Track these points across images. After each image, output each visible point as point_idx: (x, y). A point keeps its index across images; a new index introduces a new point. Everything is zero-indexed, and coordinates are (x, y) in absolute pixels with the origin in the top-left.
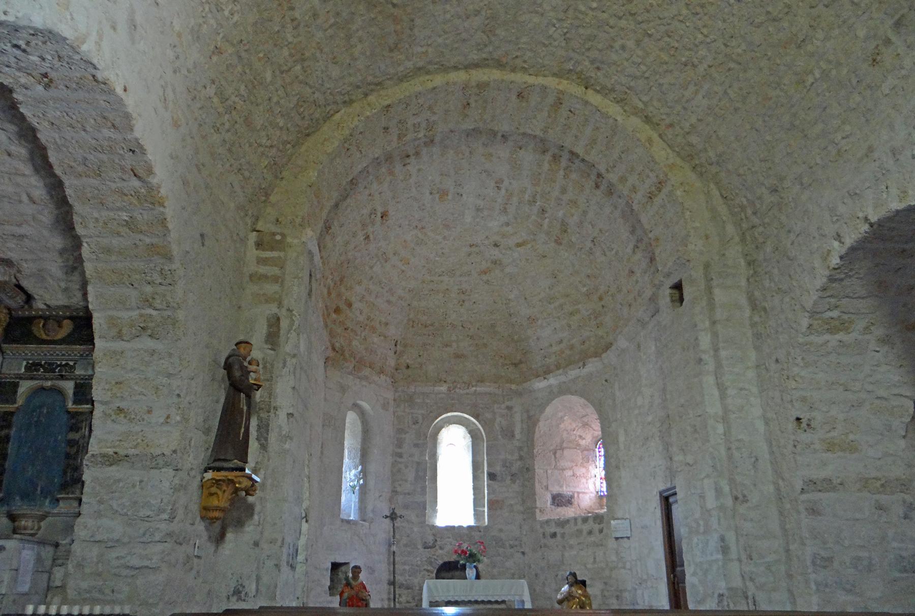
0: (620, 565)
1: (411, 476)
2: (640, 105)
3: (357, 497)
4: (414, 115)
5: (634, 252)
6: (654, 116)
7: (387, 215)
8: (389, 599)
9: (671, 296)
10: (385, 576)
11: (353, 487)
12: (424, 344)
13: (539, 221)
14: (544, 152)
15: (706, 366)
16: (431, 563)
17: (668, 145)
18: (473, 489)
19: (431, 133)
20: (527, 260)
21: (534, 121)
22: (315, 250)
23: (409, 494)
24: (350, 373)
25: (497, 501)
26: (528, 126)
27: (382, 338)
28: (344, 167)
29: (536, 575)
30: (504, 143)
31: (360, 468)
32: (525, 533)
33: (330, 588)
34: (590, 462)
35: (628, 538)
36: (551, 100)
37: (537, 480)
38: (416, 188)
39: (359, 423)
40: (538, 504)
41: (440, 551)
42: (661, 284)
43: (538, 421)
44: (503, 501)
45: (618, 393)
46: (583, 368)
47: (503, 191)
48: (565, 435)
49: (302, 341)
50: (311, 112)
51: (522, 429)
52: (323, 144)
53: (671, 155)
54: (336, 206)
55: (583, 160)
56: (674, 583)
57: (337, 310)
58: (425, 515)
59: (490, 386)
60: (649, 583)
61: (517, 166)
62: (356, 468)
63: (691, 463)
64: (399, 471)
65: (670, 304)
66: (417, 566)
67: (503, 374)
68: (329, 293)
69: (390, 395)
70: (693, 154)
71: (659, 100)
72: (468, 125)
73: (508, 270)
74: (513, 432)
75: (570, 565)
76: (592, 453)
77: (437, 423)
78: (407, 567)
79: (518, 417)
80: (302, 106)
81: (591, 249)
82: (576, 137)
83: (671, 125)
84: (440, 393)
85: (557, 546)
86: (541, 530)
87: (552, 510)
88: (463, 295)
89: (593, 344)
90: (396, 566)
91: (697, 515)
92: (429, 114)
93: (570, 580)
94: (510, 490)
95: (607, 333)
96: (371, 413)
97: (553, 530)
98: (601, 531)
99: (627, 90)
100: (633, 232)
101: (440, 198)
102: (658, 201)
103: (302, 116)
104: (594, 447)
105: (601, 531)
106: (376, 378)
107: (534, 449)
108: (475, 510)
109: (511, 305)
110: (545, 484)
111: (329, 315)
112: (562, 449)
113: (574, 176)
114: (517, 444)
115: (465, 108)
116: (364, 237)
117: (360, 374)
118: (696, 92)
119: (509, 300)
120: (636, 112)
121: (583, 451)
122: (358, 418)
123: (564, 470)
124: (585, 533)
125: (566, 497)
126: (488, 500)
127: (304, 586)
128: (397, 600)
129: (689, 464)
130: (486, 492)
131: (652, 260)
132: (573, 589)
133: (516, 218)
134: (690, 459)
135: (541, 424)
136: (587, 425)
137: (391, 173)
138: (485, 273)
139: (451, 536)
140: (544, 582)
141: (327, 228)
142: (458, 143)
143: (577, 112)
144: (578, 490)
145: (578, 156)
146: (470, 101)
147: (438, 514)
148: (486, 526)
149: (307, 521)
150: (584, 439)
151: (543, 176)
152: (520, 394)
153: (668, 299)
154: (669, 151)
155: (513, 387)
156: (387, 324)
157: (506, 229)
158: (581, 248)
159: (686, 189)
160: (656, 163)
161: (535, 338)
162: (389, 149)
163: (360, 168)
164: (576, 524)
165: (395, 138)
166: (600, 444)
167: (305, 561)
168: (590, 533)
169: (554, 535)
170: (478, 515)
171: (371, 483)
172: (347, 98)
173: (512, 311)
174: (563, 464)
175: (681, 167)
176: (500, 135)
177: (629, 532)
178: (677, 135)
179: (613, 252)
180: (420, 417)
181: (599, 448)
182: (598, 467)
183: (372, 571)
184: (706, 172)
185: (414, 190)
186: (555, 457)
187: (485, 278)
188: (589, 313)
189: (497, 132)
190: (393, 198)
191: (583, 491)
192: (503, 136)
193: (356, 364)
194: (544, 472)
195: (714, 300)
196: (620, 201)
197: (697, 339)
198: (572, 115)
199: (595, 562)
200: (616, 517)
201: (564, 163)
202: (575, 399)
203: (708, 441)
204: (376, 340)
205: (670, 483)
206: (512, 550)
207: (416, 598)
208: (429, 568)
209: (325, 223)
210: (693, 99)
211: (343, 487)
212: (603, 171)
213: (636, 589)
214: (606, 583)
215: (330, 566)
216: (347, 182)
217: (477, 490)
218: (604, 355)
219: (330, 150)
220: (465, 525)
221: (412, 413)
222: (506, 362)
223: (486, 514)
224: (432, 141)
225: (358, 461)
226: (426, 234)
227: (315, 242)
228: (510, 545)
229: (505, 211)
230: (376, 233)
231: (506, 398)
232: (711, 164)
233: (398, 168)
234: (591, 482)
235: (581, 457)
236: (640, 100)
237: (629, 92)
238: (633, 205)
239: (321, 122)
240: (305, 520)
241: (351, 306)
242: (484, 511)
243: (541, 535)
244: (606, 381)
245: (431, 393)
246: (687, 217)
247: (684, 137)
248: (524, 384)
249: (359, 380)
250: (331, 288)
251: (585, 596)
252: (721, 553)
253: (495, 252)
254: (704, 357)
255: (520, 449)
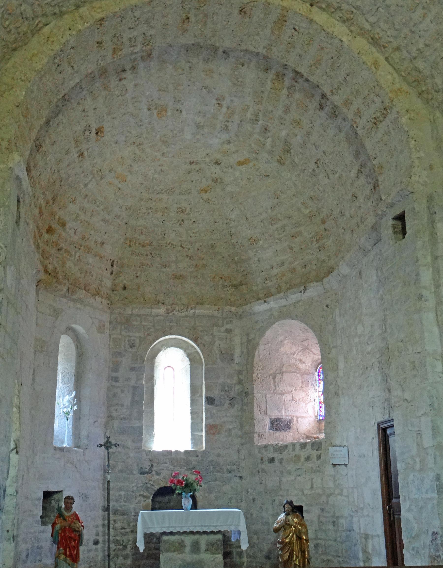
0: (337, 492)
1: (127, 400)
2: (367, 26)
3: (71, 423)
4: (130, 28)
5: (357, 177)
6: (380, 38)
7: (102, 132)
8: (104, 525)
9: (394, 226)
10: (100, 502)
11: (67, 413)
12: (142, 264)
13: (262, 139)
14: (267, 70)
15: (427, 303)
16: (147, 489)
17: (395, 69)
18: (191, 413)
19: (148, 47)
20: (249, 179)
21: (257, 38)
22: (24, 175)
23: (125, 419)
24: (64, 296)
25: (215, 426)
26: (250, 43)
27: (98, 258)
28: (55, 84)
29: (254, 500)
30: (226, 59)
31: (74, 393)
32: (243, 457)
33: (42, 517)
34: (310, 386)
35: (346, 465)
36: (274, 17)
37: (255, 405)
38: (133, 104)
39: (73, 346)
40: (257, 429)
41: (157, 477)
42: (384, 215)
43: (258, 344)
44: (221, 426)
45: (338, 319)
46: (304, 292)
47: (224, 109)
48: (285, 358)
49: (9, 277)
50: (18, 25)
51: (242, 352)
52: (31, 59)
53: (397, 80)
54: (48, 122)
55: (307, 80)
56: (389, 514)
57: (50, 230)
58: (141, 440)
59: (209, 309)
60: (365, 513)
61: (239, 83)
62: (70, 393)
63: (409, 398)
64: (115, 395)
65: (393, 236)
66: (133, 492)
67: (223, 296)
68: (41, 213)
69: (106, 318)
70: (420, 79)
71: (386, 22)
72: (187, 39)
73: (228, 189)
74: (232, 355)
75: (288, 490)
76: (312, 377)
77: (154, 346)
78: (122, 493)
79: (237, 340)
80: (7, 19)
81: (314, 170)
82: (300, 56)
83: (398, 49)
84: (157, 316)
85: (275, 472)
86: (259, 455)
87: (270, 435)
88: (182, 214)
89: (314, 268)
90: (111, 492)
91: (414, 452)
92: (146, 28)
93: (286, 509)
94: (228, 414)
95: (329, 256)
96: (87, 336)
97: (271, 455)
98: (319, 457)
99: (353, 9)
100: (357, 156)
101: (159, 114)
102: (382, 127)
103: (8, 29)
104: (314, 371)
105: (319, 457)
106: (92, 301)
107: (253, 373)
108: (192, 435)
109: (231, 225)
110: (264, 408)
111: (41, 235)
112: (282, 373)
113: (298, 96)
114: (237, 368)
115: (184, 22)
116: (78, 155)
117: (74, 297)
118: (424, 16)
119: (230, 219)
120: (362, 33)
121: (303, 374)
122: (71, 341)
123: (284, 394)
124: (302, 459)
125: (285, 421)
126: (205, 425)
127: (14, 519)
128: (111, 526)
129: (407, 400)
130: (204, 416)
131: (376, 186)
132: (290, 517)
133: (237, 136)
134: (407, 395)
135: (261, 347)
136: (307, 349)
137: (106, 88)
138: (206, 192)
139: (167, 461)
140: (261, 507)
141: (38, 146)
142: (178, 57)
143: (302, 30)
144: (298, 415)
145: (302, 76)
146: (189, 15)
147: (155, 439)
148: (204, 451)
149: (17, 452)
150: (304, 363)
151: (266, 93)
152: (240, 317)
153: (391, 231)
154: (395, 75)
155: (233, 309)
156: (103, 244)
157: (226, 146)
158: (304, 170)
159: (412, 117)
160: (381, 88)
161: (256, 259)
162: (103, 63)
163: (72, 83)
164: (294, 449)
165: (110, 53)
166: (320, 368)
167: (15, 494)
168: (308, 459)
169: (272, 460)
170: (195, 439)
171: (86, 409)
172: (57, 10)
173: (233, 231)
174: (282, 388)
175: (407, 92)
176: (221, 50)
177: (347, 459)
178: (404, 59)
179: (337, 175)
180: (137, 341)
181: (319, 372)
182: (317, 391)
183: (85, 497)
184: (432, 99)
185: (130, 105)
186: (275, 382)
187: (205, 196)
188: (310, 236)
189: (218, 48)
190: (109, 114)
191: (302, 415)
192: (224, 52)
193: (70, 286)
194: (263, 396)
195: (437, 234)
196: (344, 123)
197: (418, 274)
198: (296, 33)
199: (312, 487)
200: (334, 444)
201: (287, 82)
202: (295, 323)
203: (427, 379)
204: (91, 260)
205: (388, 415)
206: (229, 475)
207: (132, 524)
208: (145, 494)
209: (35, 141)
210: (421, 22)
211: (56, 413)
212: (328, 93)
213: (352, 517)
214: (322, 510)
215: (41, 495)
216: (59, 100)
217: (195, 414)
218: (325, 280)
219: (38, 66)
220: (182, 450)
221: (129, 336)
222: (226, 284)
223: (204, 439)
224: (149, 55)
225: (72, 386)
226: (143, 151)
227: (24, 167)
228: (228, 470)
229: (226, 129)
230: (90, 150)
231: (225, 321)
232: (437, 92)
233: (114, 82)
234: (310, 406)
235: (300, 381)
236: (367, 21)
237: (355, 11)
238: (358, 129)
239: (29, 35)
240: (14, 451)
241: (65, 225)
242: (202, 435)
243: (259, 461)
244: (327, 306)
245: (147, 315)
246: (411, 146)
247: (411, 61)
248: (244, 307)
249: (73, 303)
250: (43, 208)
251: (301, 525)
252: (436, 491)
253: (217, 170)
254: (425, 293)
255: (240, 373)
